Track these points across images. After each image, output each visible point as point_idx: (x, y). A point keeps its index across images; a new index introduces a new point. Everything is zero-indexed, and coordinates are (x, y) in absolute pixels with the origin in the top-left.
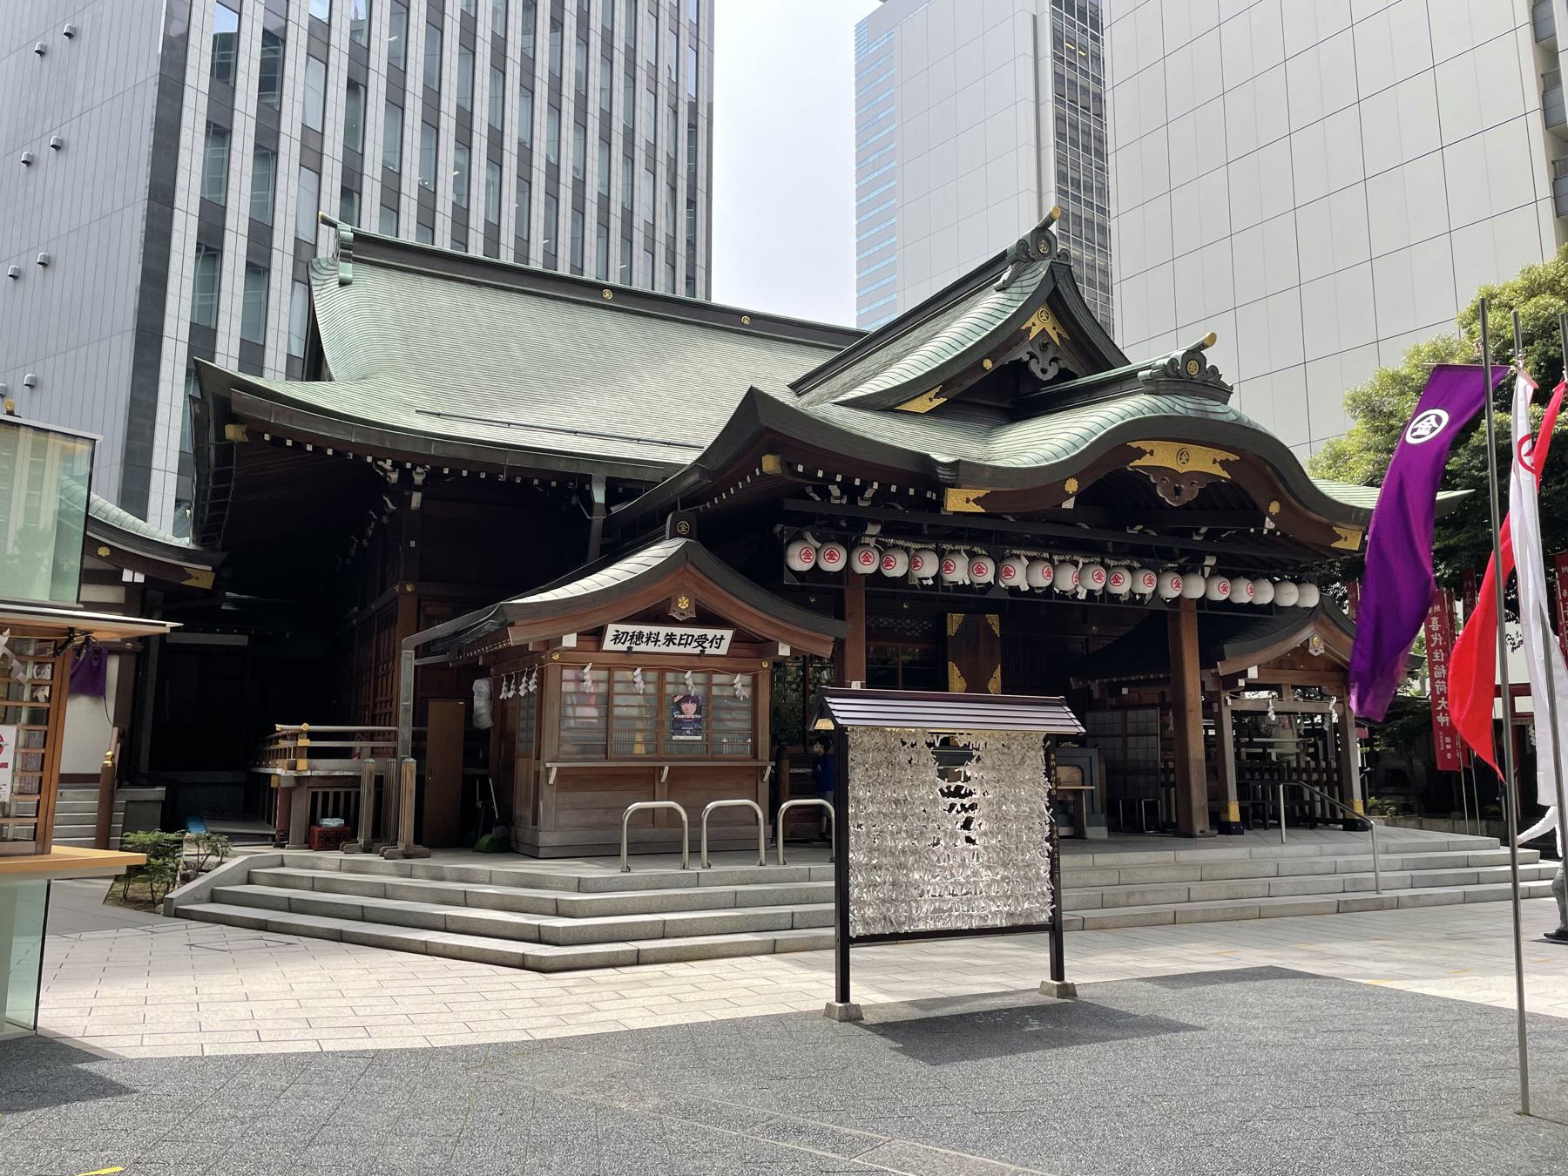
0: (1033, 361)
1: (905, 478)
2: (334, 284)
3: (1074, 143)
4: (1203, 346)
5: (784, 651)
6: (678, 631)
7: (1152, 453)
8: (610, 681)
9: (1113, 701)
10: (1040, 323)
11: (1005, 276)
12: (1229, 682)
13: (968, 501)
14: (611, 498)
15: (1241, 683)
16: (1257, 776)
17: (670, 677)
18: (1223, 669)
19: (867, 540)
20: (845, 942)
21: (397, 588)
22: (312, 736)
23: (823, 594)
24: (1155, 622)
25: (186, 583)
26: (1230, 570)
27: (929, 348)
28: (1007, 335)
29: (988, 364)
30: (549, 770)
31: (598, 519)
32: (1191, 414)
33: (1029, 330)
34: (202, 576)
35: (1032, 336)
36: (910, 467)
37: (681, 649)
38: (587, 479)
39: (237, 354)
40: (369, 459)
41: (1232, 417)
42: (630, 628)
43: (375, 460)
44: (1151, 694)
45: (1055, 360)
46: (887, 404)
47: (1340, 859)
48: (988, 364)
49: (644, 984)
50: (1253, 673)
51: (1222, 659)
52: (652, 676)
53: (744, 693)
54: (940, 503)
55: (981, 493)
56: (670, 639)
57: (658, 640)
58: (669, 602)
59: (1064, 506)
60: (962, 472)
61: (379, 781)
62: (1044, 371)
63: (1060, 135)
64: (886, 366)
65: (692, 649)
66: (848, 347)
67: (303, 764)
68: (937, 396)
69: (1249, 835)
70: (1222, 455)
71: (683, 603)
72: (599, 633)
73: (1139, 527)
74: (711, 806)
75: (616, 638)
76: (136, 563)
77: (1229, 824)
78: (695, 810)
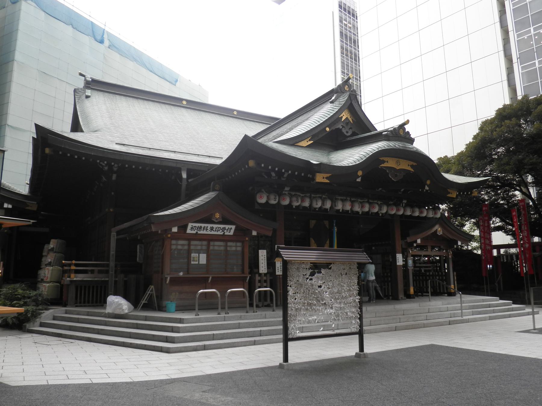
0: (343, 129)
2: (84, 97)
3: (347, 55)
4: (405, 124)
5: (254, 233)
6: (215, 226)
7: (387, 162)
8: (189, 245)
10: (345, 115)
11: (333, 98)
13: (324, 178)
14: (189, 176)
15: (415, 245)
18: (409, 240)
20: (286, 340)
21: (107, 210)
22: (76, 265)
23: (269, 212)
24: (385, 222)
25: (27, 208)
26: (411, 205)
27: (307, 123)
28: (334, 120)
29: (328, 129)
30: (166, 278)
31: (184, 184)
33: (342, 117)
34: (33, 206)
37: (216, 233)
38: (180, 169)
40: (98, 161)
41: (415, 149)
43: (100, 161)
45: (351, 128)
46: (293, 142)
47: (449, 306)
48: (328, 129)
49: (208, 357)
50: (419, 241)
53: (239, 249)
54: (313, 179)
55: (328, 175)
56: (212, 229)
57: (207, 229)
58: (213, 215)
59: (357, 180)
60: (322, 167)
61: (126, 282)
62: (347, 132)
63: (342, 53)
64: (291, 129)
66: (275, 124)
67: (73, 275)
68: (310, 140)
69: (416, 299)
71: (217, 215)
72: (185, 227)
73: (380, 189)
74: (201, 291)
75: (192, 229)
76: (9, 201)
78: (223, 292)
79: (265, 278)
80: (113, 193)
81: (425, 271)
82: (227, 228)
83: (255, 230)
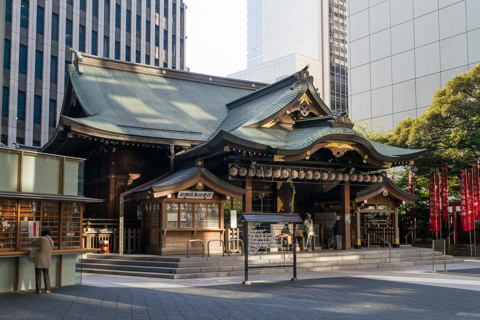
0: (302, 110)
1: (263, 151)
6: (198, 193)
9: (328, 210)
12: (359, 204)
15: (363, 205)
16: (374, 232)
17: (196, 206)
18: (357, 201)
19: (251, 167)
32: (342, 133)
35: (301, 103)
36: (264, 149)
37: (199, 198)
39: (17, 79)
42: (185, 192)
44: (336, 207)
45: (308, 110)
50: (366, 202)
51: (356, 198)
52: (190, 205)
54: (273, 158)
56: (196, 195)
62: (305, 113)
65: (202, 197)
70: (352, 143)
71: (200, 184)
77: (357, 246)
79: (235, 232)
80: (113, 163)
81: (381, 226)
82: (207, 194)
83: (229, 195)
